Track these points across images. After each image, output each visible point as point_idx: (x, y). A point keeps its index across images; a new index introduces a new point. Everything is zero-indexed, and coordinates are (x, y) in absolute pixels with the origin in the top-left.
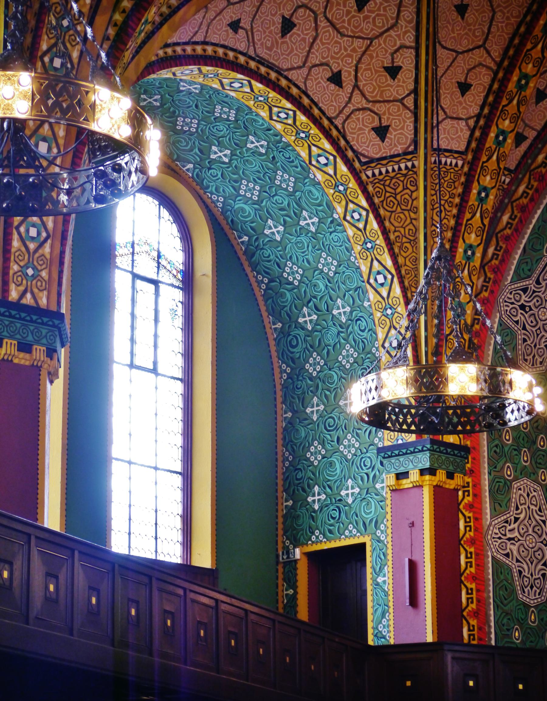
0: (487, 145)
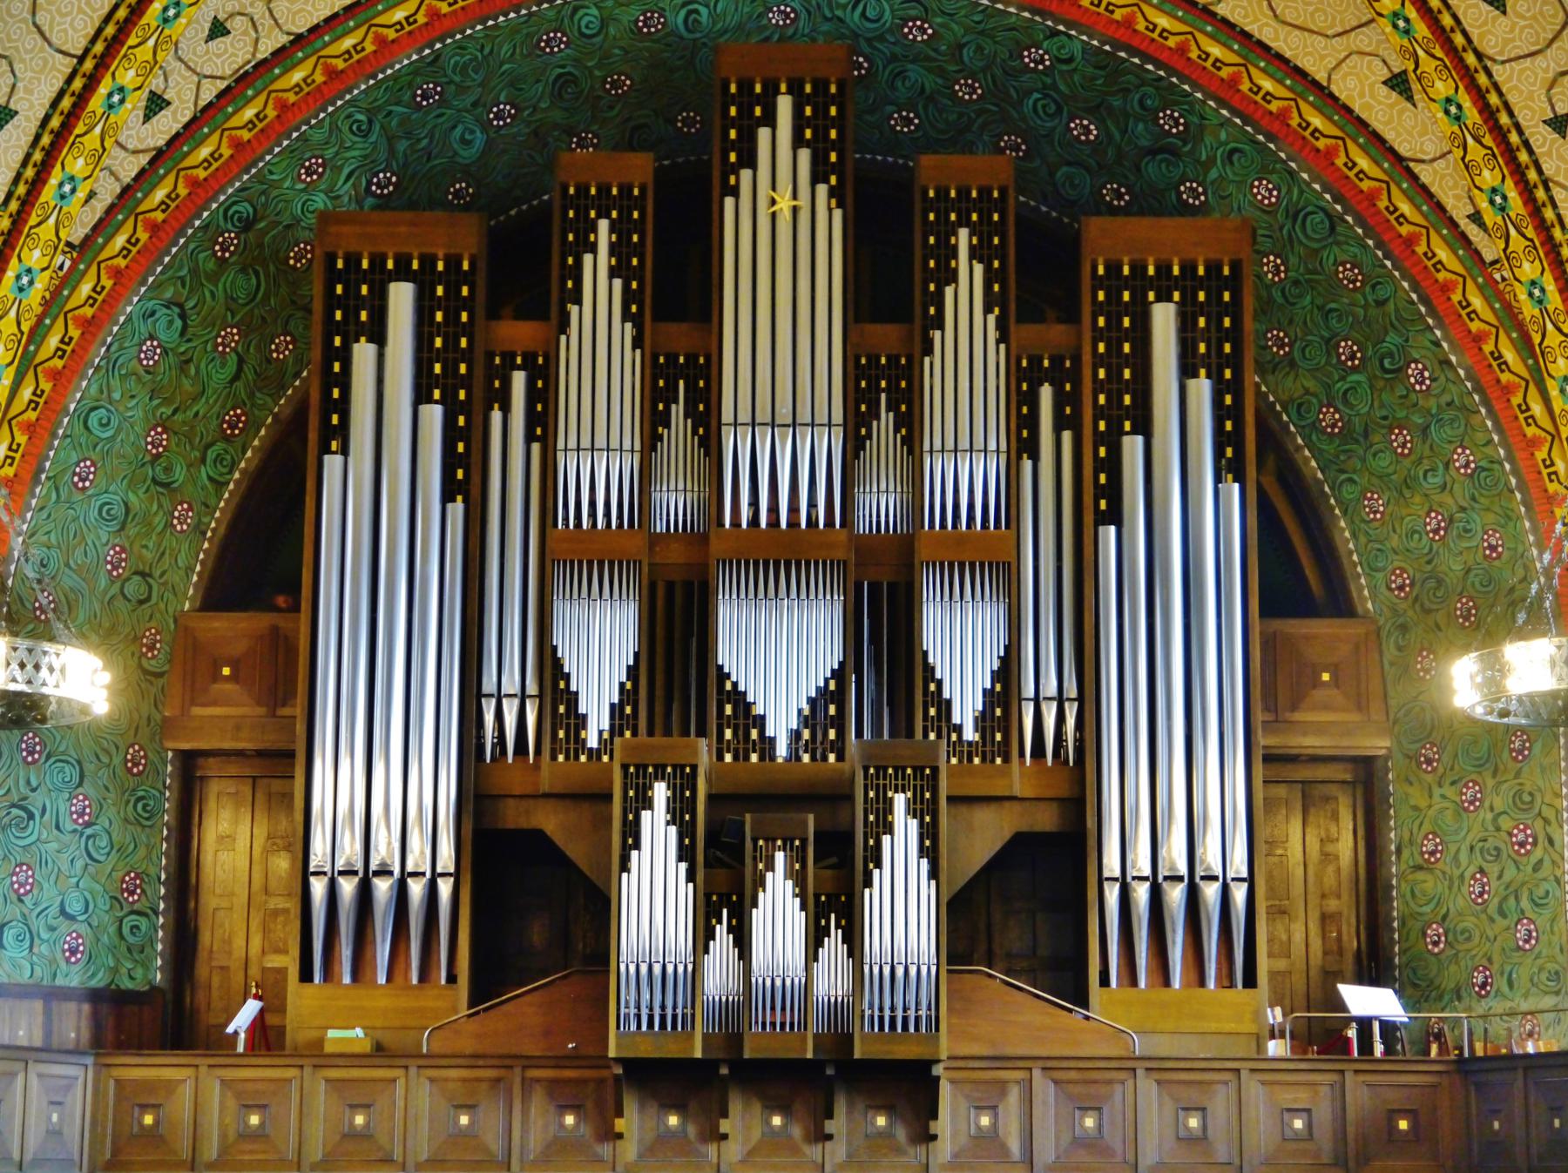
0: (42, 199)
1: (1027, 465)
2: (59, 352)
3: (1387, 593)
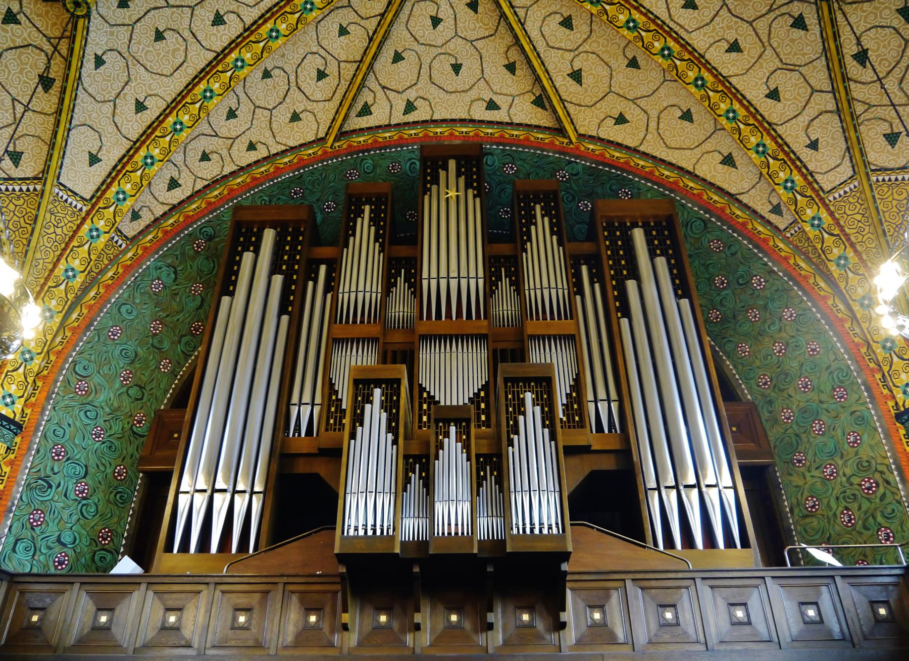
1: (578, 298)
2: (112, 278)
3: (758, 389)
